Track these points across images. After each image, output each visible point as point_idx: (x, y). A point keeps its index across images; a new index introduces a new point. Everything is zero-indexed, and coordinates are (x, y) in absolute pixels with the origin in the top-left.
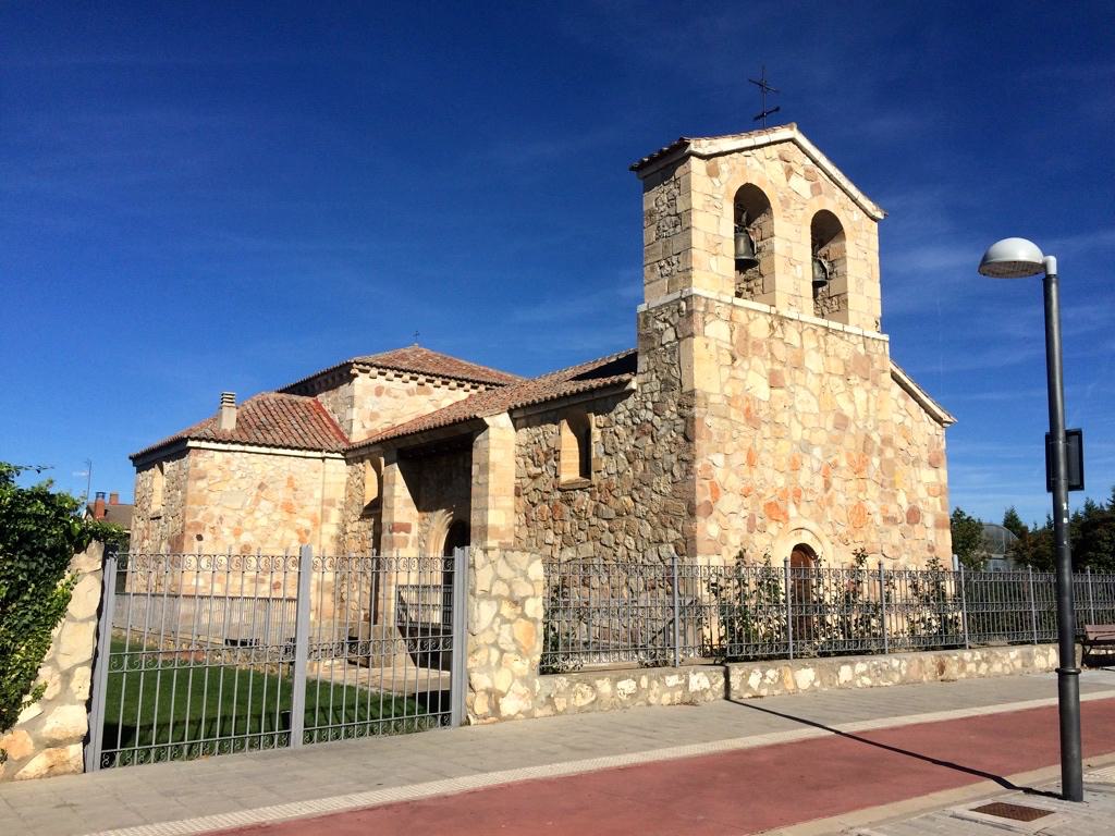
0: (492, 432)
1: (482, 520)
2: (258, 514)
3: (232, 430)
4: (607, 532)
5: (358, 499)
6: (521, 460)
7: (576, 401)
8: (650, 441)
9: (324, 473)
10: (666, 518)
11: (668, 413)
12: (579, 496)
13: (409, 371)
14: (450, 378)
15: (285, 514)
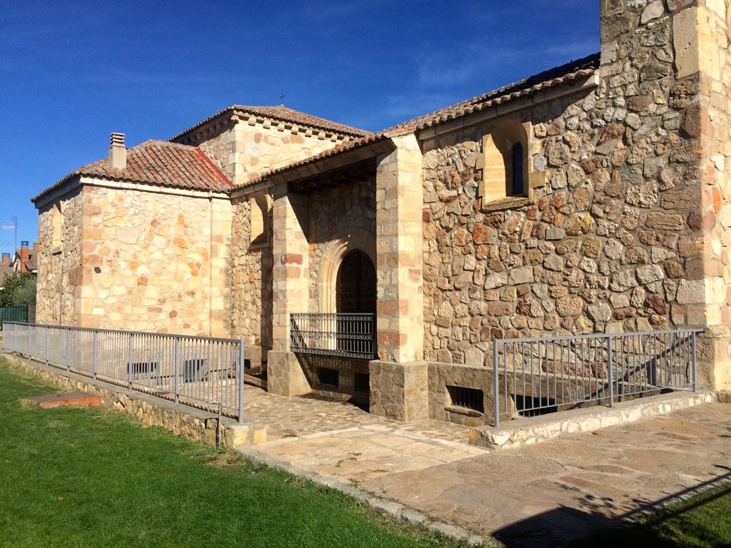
0: (400, 153)
1: (391, 247)
2: (151, 249)
3: (123, 169)
4: (553, 255)
5: (244, 235)
6: (431, 184)
7: (509, 110)
8: (620, 144)
9: (212, 211)
10: (648, 234)
11: (652, 108)
12: (511, 216)
13: (284, 120)
14: (319, 128)
15: (178, 249)
